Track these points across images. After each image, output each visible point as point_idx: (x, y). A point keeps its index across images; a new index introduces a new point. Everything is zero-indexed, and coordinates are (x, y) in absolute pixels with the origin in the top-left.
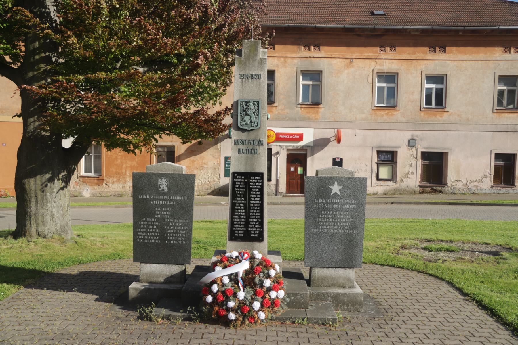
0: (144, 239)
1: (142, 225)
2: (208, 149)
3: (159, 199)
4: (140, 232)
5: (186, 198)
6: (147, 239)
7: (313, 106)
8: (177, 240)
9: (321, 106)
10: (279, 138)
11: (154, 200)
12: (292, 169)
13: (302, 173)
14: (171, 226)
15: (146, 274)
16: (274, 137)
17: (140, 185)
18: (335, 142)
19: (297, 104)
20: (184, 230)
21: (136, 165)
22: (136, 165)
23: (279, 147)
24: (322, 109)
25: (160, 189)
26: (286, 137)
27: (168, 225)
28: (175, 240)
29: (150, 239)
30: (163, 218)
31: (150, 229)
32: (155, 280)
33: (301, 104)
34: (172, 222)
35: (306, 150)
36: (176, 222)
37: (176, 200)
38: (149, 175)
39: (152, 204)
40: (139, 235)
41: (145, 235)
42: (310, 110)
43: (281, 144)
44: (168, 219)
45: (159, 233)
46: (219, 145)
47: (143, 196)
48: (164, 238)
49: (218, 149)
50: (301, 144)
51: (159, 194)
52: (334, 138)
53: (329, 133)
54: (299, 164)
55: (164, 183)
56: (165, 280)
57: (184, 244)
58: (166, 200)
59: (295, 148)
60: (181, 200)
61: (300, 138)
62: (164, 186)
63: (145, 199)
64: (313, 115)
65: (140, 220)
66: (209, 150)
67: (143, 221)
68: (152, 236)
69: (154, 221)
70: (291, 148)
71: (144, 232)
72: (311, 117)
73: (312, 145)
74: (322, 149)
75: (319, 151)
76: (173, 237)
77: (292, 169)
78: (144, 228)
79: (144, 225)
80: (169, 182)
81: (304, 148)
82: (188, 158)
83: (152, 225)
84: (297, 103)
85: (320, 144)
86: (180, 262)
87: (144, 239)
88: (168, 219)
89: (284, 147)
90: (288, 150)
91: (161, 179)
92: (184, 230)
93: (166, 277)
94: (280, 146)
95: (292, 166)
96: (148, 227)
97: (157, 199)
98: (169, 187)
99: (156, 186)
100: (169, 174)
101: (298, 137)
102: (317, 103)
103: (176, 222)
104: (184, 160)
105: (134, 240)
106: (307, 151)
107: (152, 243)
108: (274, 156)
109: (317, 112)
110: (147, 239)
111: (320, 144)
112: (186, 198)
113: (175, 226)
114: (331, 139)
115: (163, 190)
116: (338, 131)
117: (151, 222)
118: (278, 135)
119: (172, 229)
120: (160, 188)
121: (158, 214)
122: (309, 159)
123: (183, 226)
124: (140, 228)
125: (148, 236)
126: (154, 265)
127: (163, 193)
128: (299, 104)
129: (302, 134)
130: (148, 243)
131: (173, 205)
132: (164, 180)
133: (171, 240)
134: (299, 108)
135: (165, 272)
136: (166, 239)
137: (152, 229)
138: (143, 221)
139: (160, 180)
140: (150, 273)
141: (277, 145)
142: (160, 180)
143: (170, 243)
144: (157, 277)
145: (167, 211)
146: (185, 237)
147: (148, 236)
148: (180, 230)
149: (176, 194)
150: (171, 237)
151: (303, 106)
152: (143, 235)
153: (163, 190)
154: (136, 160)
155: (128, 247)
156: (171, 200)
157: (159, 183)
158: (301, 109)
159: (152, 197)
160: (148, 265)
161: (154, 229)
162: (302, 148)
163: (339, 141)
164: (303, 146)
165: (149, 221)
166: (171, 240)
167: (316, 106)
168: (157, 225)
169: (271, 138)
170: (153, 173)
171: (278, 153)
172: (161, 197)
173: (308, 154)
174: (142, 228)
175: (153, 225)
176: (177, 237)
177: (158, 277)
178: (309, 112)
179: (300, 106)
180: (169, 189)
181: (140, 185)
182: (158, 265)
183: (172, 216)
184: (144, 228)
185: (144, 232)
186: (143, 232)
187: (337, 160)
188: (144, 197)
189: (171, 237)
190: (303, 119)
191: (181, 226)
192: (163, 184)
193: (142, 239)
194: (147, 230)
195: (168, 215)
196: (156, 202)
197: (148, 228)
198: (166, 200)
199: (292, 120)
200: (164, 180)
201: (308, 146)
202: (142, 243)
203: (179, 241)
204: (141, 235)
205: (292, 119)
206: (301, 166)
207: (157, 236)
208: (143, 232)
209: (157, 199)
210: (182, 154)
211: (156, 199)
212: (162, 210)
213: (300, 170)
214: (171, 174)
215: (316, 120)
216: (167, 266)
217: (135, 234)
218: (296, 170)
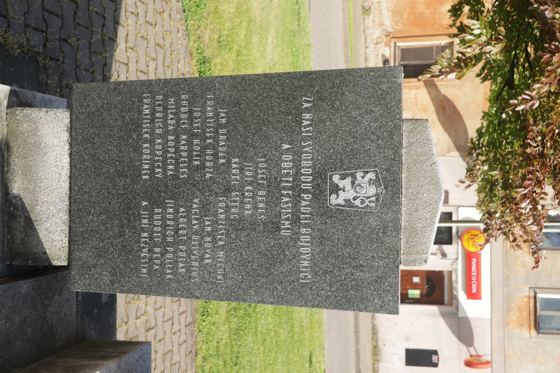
0: (153, 120)
1: (204, 112)
2: (449, 134)
3: (297, 174)
4: (178, 106)
5: (306, 276)
6: (152, 133)
7: (532, 318)
8: (152, 244)
9: (533, 332)
10: (470, 258)
11: (297, 153)
12: (416, 280)
13: (410, 296)
14: (201, 222)
15: (35, 131)
16: (472, 249)
17: (350, 97)
18: (467, 357)
19: (535, 291)
20: (189, 269)
21: (418, 11)
22: (418, 11)
23: (455, 256)
24: (527, 334)
25: (336, 178)
26: (474, 269)
27: (206, 209)
28: (151, 237)
29: (152, 142)
30: (228, 190)
31: (190, 143)
32: (16, 162)
33: (535, 298)
34: (215, 223)
35: (451, 304)
36: (214, 241)
37: (296, 237)
38: (391, 134)
39: (278, 147)
40: (165, 99)
41: (166, 125)
42: (525, 314)
43: (460, 261)
44: (227, 209)
45: (175, 177)
46: (457, 154)
47: (308, 110)
48: (158, 193)
49: (449, 151)
50: (462, 296)
51: (321, 175)
52: (474, 353)
53: (483, 346)
54: (425, 292)
55: (362, 193)
56: (18, 198)
57: (138, 271)
58: (296, 200)
59: (454, 285)
60: (296, 256)
61: (473, 295)
62: (349, 194)
63: (299, 122)
64: (515, 319)
65: (219, 102)
66: (446, 136)
67: (217, 115)
68: (165, 150)
69: (215, 156)
70: (454, 278)
71: (178, 120)
72: (511, 313)
73: (460, 315)
74: (454, 332)
75: (450, 326)
76: (164, 226)
77: (416, 280)
78: (191, 119)
79: (205, 120)
80: (367, 212)
81: (454, 301)
82: (433, 100)
83: (204, 148)
84: (537, 290)
85: (463, 330)
86: (77, 254)
87: (153, 120)
88: (227, 209)
89: (454, 267)
90: (450, 273)
91: (376, 182)
92: (189, 269)
93: (26, 201)
94: (457, 259)
95: (422, 279)
96: (196, 136)
97: (297, 166)
98: (346, 212)
99: (349, 165)
100: (399, 212)
101: (474, 291)
102: (538, 325)
103: (214, 241)
104: (427, 95)
105: (148, 85)
106: (448, 305)
107: (138, 150)
108: (438, 250)
109: (522, 325)
110: (152, 133)
111: (463, 330)
112: (306, 276)
113: (201, 234)
114: (471, 349)
115: (336, 189)
116: (488, 363)
117: (214, 147)
118: (477, 256)
119: (189, 222)
120: (343, 178)
121: (242, 170)
122: (434, 309)
123: (202, 267)
124: (191, 102)
125: (164, 136)
126: (66, 160)
127: (322, 188)
128: (535, 294)
129: (480, 298)
130: (140, 135)
131: (278, 229)
132: (372, 191)
133: (151, 219)
134: (527, 292)
135: (42, 198)
136: (156, 202)
137: (190, 151)
138: (217, 115)
139: (371, 176)
140: (37, 145)
141: (458, 253)
142: (371, 176)
143: (139, 217)
144: (28, 172)
145: (251, 205)
146: (163, 273)
147: (164, 136)
148: (189, 253)
149: (321, 239)
150: (164, 219)
151: (532, 301)
152: (165, 118)
153: (336, 189)
154: (427, 11)
155: (227, 25)
156: (295, 220)
157: (359, 175)
158: (525, 297)
159: (308, 147)
160: (65, 136)
161: (190, 157)
162: (453, 298)
163: (469, 364)
164: (457, 299)
165: (216, 139)
166: (151, 219)
167: (532, 323)
168: (203, 167)
169: (471, 244)
170: (400, 145)
171: (444, 255)
172: (307, 180)
173: (444, 308)
174: (191, 112)
175: (202, 154)
176: (164, 245)
177: (24, 174)
178: (520, 310)
179: (532, 294)
180: (339, 210)
181: (350, 97)
182: (66, 172)
183: (237, 225)
184: (191, 119)
185: (178, 120)
186: (177, 114)
187: (434, 358)
188: (307, 116)
189: (164, 219)
190: (508, 300)
191: (202, 259)
192: (356, 190)
193: (153, 113)
194: (185, 131)
195: (242, 208)
196: (287, 164)
197: (192, 135)
198: (296, 200)
199: (506, 279)
200: (372, 191)
201: (457, 310)
202: (140, 112)
203: (150, 251)
204: (165, 109)
205: (507, 279)
206: (422, 294)
207: (165, 170)
208: (177, 114)
209: (297, 166)
210: (438, 90)
211: (296, 161)
212: (259, 186)
213: (415, 293)
214: (397, 221)
215: (506, 323)
216: (65, 204)
217: (170, 88)
218: (415, 286)
